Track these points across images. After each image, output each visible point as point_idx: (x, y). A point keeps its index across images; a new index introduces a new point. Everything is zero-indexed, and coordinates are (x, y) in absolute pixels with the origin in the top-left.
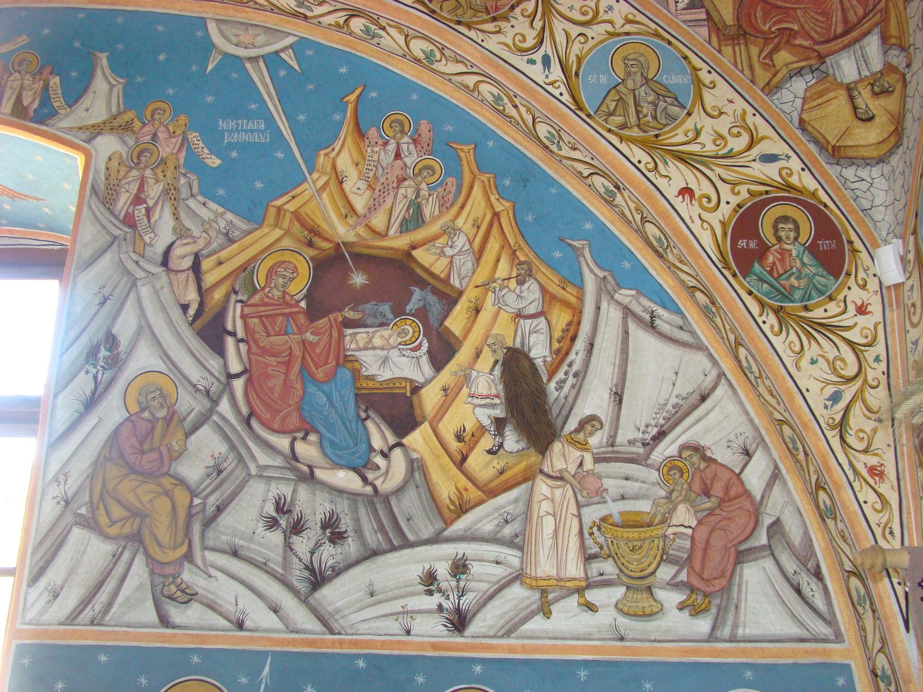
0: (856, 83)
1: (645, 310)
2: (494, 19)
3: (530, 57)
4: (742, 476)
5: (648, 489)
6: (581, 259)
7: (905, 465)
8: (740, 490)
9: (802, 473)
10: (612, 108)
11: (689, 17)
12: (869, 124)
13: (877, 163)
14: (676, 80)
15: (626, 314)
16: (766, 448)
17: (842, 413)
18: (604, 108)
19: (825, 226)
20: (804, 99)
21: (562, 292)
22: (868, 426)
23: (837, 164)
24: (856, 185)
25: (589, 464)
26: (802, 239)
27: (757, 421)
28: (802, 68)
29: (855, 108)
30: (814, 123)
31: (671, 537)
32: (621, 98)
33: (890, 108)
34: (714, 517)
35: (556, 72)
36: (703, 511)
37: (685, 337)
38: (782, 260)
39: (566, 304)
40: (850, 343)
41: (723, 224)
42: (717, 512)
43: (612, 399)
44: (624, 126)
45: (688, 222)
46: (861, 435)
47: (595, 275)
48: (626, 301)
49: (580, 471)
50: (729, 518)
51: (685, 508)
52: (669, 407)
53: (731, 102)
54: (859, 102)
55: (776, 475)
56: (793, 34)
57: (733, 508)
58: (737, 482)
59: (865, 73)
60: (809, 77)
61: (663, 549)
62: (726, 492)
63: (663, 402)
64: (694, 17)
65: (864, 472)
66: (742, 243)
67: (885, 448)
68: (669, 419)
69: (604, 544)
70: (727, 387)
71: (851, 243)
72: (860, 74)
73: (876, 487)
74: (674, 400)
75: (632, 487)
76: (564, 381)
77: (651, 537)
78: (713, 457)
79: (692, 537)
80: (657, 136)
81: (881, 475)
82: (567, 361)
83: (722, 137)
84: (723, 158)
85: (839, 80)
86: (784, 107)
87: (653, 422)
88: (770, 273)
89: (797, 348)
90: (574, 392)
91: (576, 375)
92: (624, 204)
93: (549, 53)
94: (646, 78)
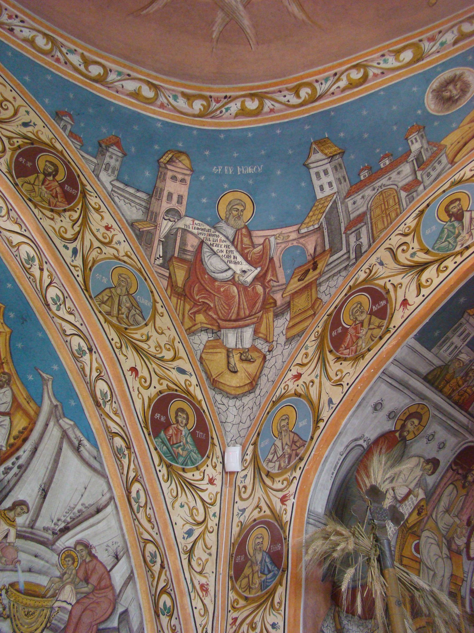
0: (233, 349)
1: (76, 438)
2: (52, 211)
3: (66, 244)
4: (111, 573)
5: (49, 568)
6: (45, 387)
7: (220, 588)
8: (108, 583)
9: (151, 580)
10: (105, 299)
11: (159, 271)
12: (234, 374)
13: (233, 398)
14: (145, 302)
15: (64, 436)
16: (129, 557)
17: (191, 544)
18: (100, 297)
19: (202, 424)
20: (205, 346)
21: (26, 404)
22: (204, 556)
23: (214, 390)
24: (220, 406)
25: (12, 538)
26: (189, 426)
27: (127, 537)
28: (208, 329)
29: (229, 363)
30: (207, 362)
31: (57, 609)
32: (112, 296)
33: (250, 370)
34: (88, 600)
35: (79, 261)
36: (82, 593)
37: (96, 465)
38: (176, 435)
39: (26, 413)
40: (203, 500)
41: (150, 399)
42: (91, 596)
43: (40, 493)
44: (109, 314)
45: (131, 390)
46: (200, 562)
47: (51, 401)
48: (66, 427)
49: (4, 541)
50: (97, 603)
51: (70, 589)
52: (76, 510)
53: (169, 329)
54: (232, 360)
55: (131, 578)
56: (209, 308)
57: (100, 595)
58: (107, 576)
59: (239, 346)
60: (210, 335)
61: (49, 618)
62: (99, 583)
63: (72, 506)
64: (162, 272)
65: (198, 587)
66: (157, 416)
67: (211, 573)
68: (74, 519)
69: (7, 606)
70: (113, 507)
71: (212, 438)
72: (236, 346)
73: (203, 598)
74: (79, 507)
75: (39, 564)
76: (10, 469)
77: (42, 606)
78: (96, 554)
79: (71, 612)
80: (126, 329)
81: (207, 591)
82: (16, 455)
83: (160, 347)
84: (158, 359)
85: (225, 344)
86: (194, 345)
87: (63, 519)
88: (169, 440)
89: (175, 494)
90: (15, 479)
91: (20, 467)
92: (89, 363)
93: (78, 248)
94: (128, 292)
